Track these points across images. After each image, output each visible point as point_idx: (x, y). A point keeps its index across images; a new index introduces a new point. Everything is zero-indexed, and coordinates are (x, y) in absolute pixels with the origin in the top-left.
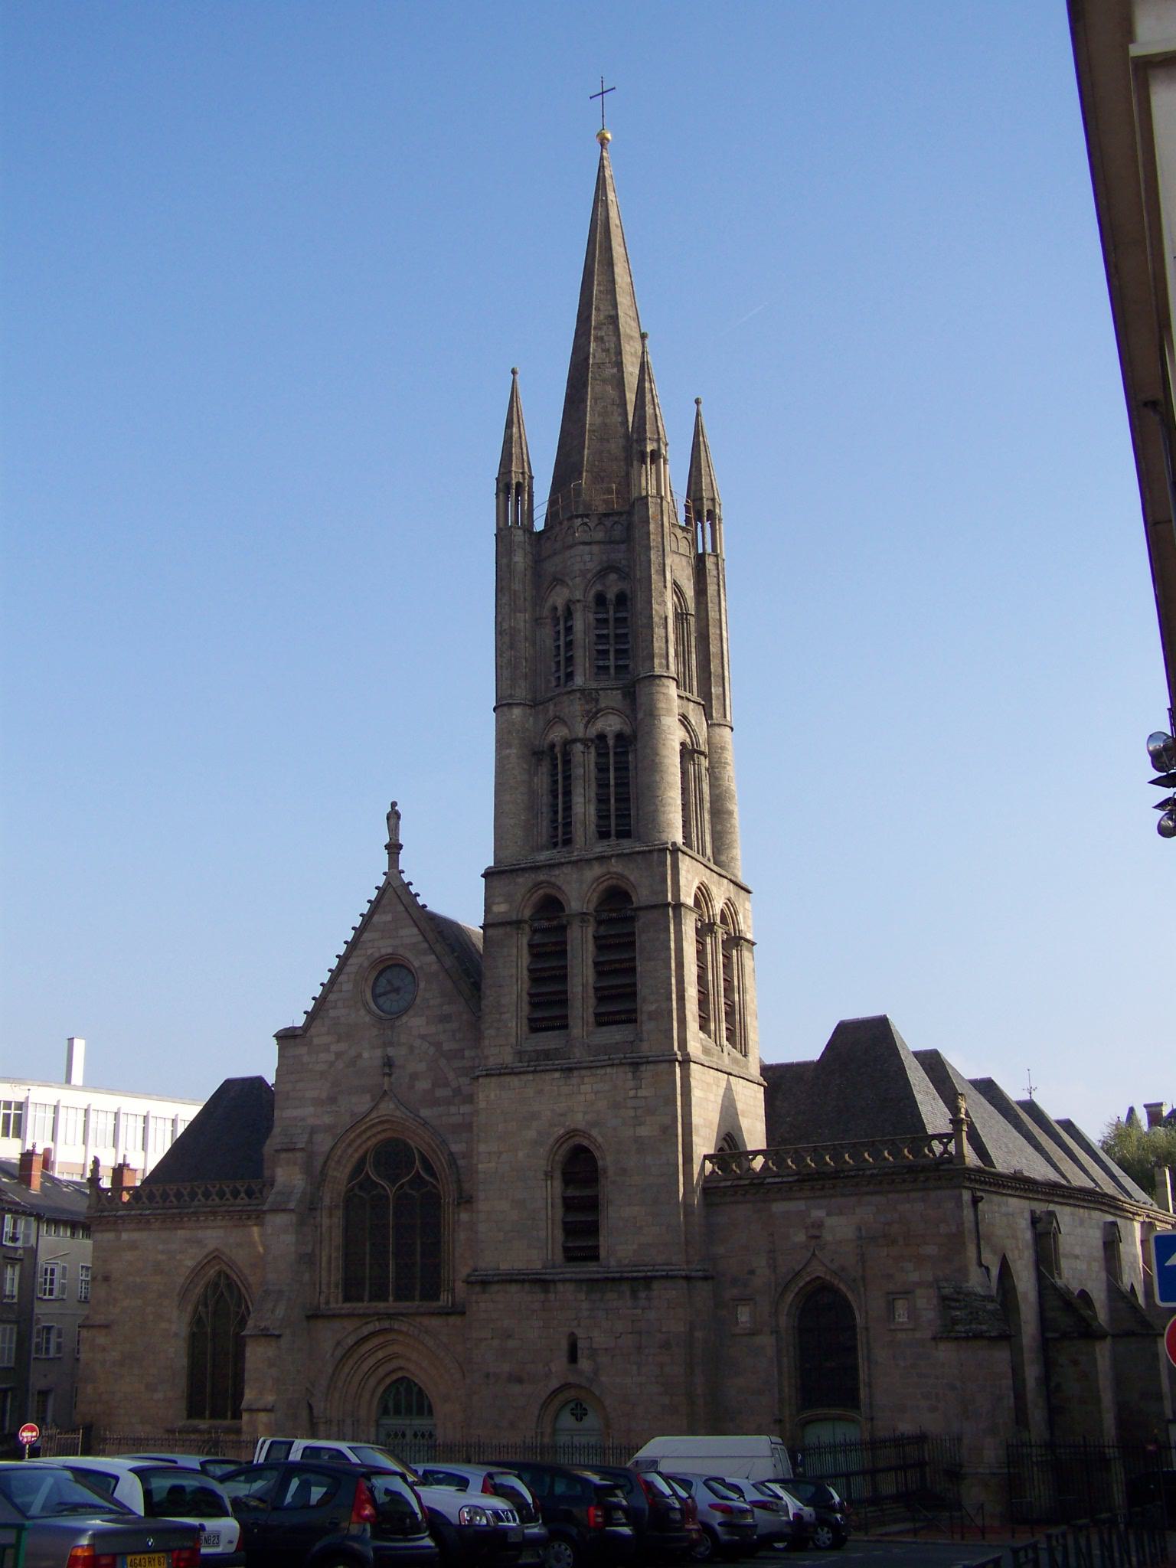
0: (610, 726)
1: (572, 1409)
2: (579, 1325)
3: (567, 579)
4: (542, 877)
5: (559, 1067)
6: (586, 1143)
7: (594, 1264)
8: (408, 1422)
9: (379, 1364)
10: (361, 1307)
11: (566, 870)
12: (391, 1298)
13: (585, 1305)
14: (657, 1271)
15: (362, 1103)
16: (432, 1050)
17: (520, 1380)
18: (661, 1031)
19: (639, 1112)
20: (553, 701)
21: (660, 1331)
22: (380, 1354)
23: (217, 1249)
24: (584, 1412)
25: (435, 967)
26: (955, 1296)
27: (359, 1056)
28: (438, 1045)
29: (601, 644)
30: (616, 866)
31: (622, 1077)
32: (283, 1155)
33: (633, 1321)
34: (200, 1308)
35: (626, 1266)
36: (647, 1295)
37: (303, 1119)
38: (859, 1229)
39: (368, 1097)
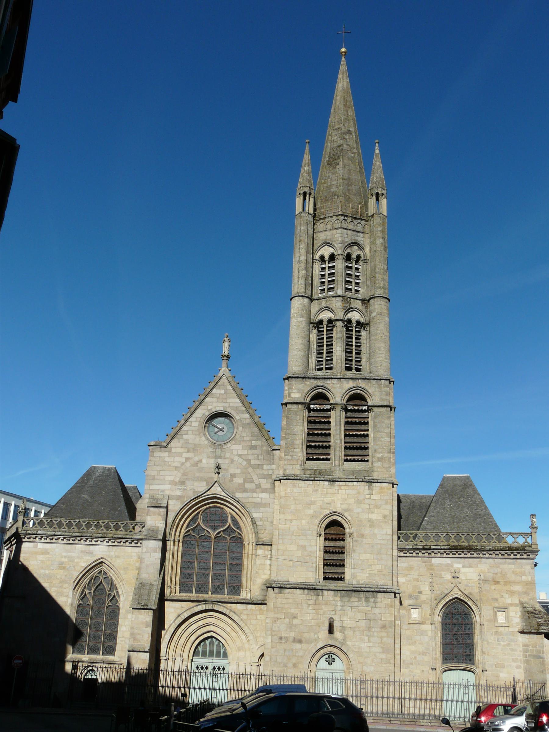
0: (354, 317)
1: (327, 658)
2: (335, 614)
3: (334, 243)
4: (319, 383)
5: (328, 479)
6: (339, 519)
7: (341, 582)
8: (211, 661)
9: (200, 628)
10: (193, 596)
11: (335, 381)
12: (210, 593)
13: (339, 604)
14: (380, 588)
15: (201, 487)
16: (244, 463)
17: (300, 641)
18: (384, 467)
19: (372, 506)
20: (325, 299)
21: (381, 620)
22: (201, 623)
23: (102, 558)
24: (333, 660)
25: (249, 421)
26: (534, 612)
27: (200, 461)
28: (248, 461)
29: (330, 285)
30: (361, 383)
31: (363, 487)
32: (152, 509)
33: (366, 613)
34: (86, 590)
35: (362, 584)
36: (374, 600)
37: (163, 491)
38: (480, 575)
39: (205, 483)
